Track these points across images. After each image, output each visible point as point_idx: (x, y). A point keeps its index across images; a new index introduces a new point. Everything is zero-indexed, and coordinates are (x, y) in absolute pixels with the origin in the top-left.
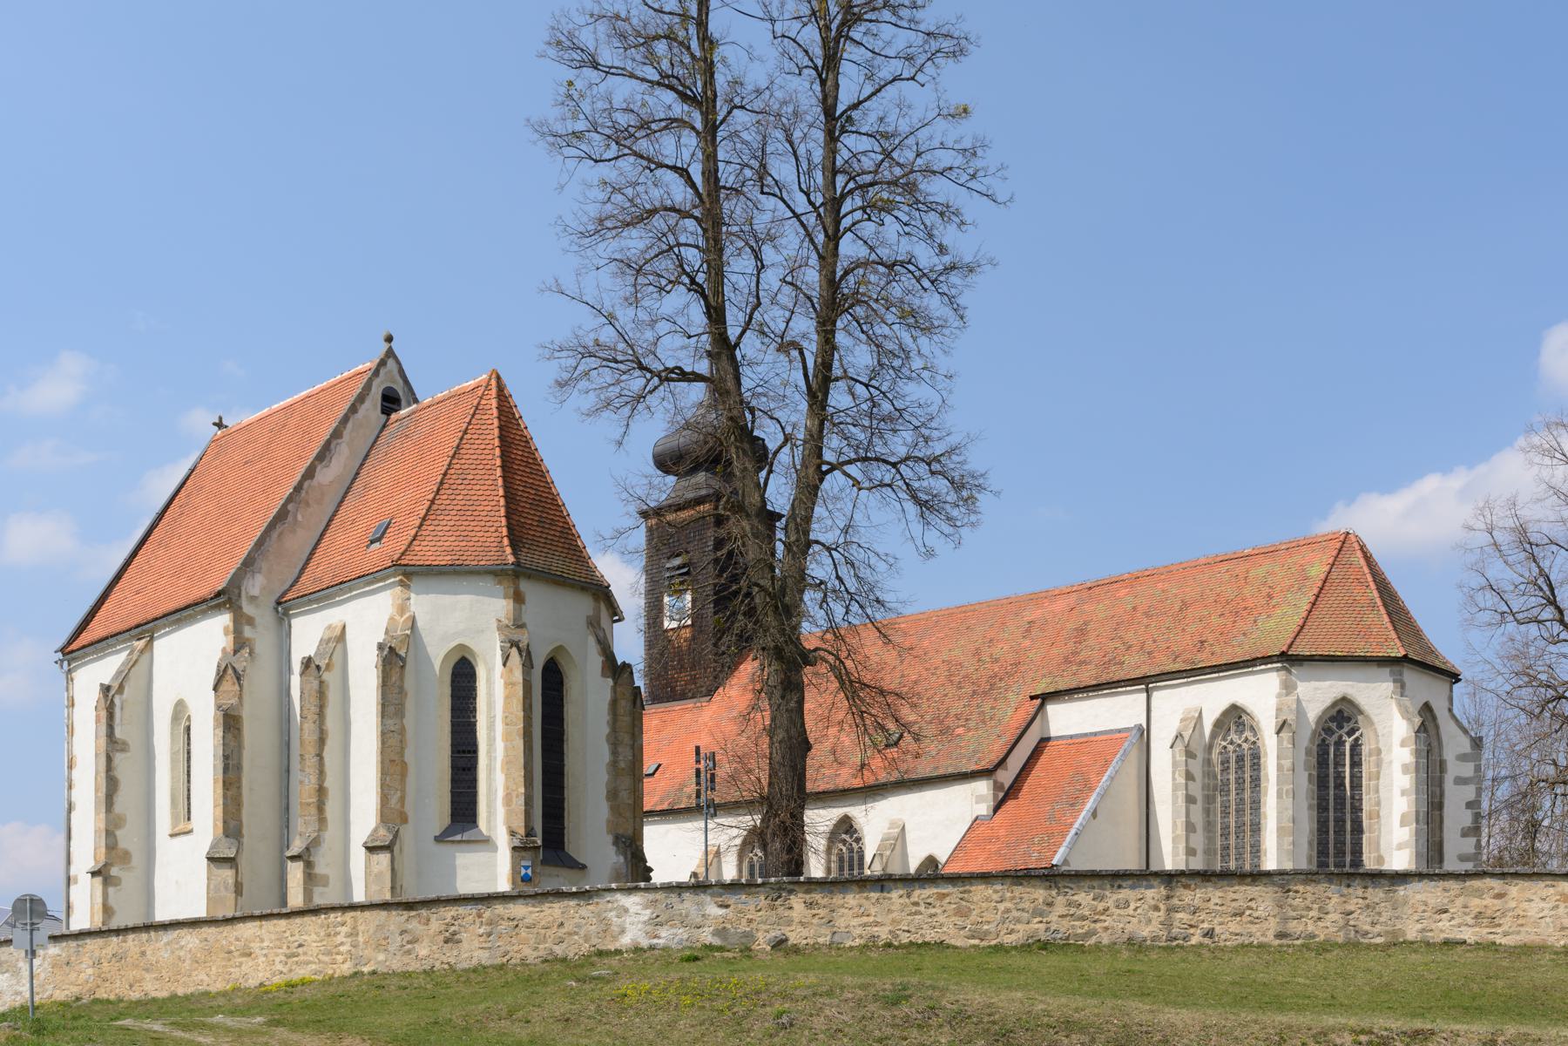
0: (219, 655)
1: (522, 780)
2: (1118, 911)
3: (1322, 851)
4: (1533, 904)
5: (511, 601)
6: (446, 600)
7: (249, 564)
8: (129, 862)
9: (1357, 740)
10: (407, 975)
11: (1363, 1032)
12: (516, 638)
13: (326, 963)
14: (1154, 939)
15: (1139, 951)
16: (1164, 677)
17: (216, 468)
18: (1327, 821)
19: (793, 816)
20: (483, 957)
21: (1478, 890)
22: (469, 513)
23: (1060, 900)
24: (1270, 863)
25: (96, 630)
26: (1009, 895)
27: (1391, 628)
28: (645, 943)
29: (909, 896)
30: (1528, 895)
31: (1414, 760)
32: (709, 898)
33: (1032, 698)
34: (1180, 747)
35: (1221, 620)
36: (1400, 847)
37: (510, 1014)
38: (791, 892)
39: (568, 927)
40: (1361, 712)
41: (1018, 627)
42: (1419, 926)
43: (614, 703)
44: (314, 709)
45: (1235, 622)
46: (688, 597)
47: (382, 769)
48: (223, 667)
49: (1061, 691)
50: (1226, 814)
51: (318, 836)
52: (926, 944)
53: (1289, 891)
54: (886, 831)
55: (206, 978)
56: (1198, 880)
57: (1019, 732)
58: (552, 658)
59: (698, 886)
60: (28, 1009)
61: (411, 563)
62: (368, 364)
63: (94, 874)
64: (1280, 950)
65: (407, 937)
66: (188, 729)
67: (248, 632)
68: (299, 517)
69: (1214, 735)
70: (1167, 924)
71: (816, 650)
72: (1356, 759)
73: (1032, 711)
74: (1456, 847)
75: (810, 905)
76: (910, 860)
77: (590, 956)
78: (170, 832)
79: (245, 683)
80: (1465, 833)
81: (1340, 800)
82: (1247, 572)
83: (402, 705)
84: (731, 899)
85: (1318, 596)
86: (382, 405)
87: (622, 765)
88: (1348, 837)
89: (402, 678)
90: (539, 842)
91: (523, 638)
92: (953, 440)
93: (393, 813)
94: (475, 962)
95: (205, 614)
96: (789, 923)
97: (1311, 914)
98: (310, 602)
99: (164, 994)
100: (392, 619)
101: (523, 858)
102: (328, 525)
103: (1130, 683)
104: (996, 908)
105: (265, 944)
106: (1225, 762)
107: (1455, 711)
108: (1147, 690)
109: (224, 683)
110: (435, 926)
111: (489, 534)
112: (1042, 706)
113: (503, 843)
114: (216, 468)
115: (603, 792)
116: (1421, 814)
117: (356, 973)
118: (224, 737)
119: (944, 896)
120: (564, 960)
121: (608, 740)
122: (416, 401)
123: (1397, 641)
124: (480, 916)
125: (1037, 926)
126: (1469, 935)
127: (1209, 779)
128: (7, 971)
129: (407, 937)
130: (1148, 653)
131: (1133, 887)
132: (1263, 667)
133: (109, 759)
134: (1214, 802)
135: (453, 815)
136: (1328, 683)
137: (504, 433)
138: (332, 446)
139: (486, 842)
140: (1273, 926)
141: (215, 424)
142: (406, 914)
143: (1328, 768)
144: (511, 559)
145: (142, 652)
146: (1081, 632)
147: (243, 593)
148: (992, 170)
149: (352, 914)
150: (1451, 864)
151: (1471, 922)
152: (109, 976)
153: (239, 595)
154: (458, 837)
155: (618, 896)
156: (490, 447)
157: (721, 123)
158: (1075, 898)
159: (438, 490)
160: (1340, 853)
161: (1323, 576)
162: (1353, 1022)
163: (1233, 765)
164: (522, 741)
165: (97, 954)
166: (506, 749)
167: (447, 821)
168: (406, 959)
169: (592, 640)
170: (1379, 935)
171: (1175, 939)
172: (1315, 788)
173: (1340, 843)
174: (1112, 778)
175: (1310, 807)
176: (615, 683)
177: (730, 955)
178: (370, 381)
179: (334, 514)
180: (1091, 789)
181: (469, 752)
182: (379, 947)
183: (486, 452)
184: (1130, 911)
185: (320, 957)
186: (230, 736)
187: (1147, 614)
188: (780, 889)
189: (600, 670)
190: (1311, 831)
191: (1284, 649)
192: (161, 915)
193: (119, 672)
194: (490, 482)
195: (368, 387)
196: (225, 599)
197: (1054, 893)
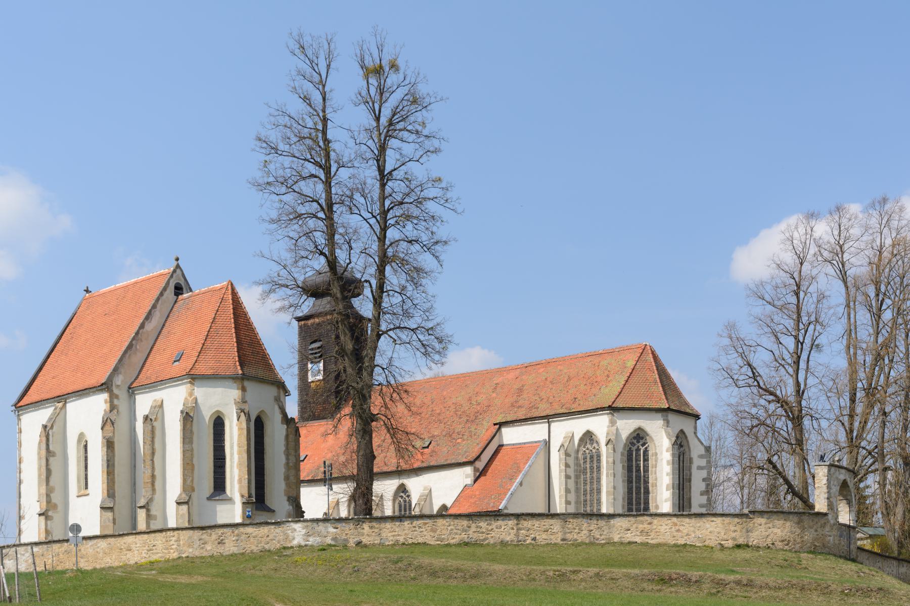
0: (103, 413)
2: (497, 530)
3: (630, 503)
4: (662, 527)
5: (240, 391)
6: (211, 390)
7: (116, 370)
8: (57, 509)
9: (646, 448)
10: (202, 558)
11: (558, 571)
12: (243, 408)
13: (165, 553)
14: (512, 541)
15: (504, 546)
16: (556, 416)
17: (88, 315)
19: (367, 489)
20: (235, 550)
21: (642, 521)
22: (220, 350)
24: (604, 510)
25: (31, 397)
26: (452, 523)
27: (663, 394)
28: (303, 543)
29: (412, 524)
30: (661, 523)
31: (671, 458)
32: (330, 525)
33: (495, 424)
34: (562, 451)
35: (585, 387)
36: (666, 501)
37: (254, 568)
38: (363, 522)
41: (490, 386)
43: (287, 436)
44: (150, 439)
45: (591, 388)
46: (321, 365)
47: (184, 467)
48: (105, 419)
50: (585, 484)
52: (419, 543)
53: (566, 521)
54: (422, 492)
55: (110, 560)
56: (530, 517)
57: (487, 442)
59: (326, 520)
60: (33, 573)
62: (167, 270)
63: (40, 515)
64: (561, 546)
65: (202, 542)
67: (116, 402)
68: (138, 347)
69: (579, 445)
70: (517, 535)
71: (378, 414)
72: (646, 458)
73: (494, 431)
74: (697, 501)
75: (371, 528)
77: (280, 549)
78: (77, 495)
80: (702, 494)
81: (638, 478)
82: (600, 362)
83: (192, 438)
84: (339, 525)
85: (629, 377)
87: (291, 464)
88: (642, 495)
89: (192, 426)
90: (254, 500)
91: (246, 407)
92: (438, 320)
93: (188, 487)
94: (231, 552)
95: (94, 393)
96: (363, 535)
97: (575, 531)
98: (146, 388)
99: (89, 568)
100: (186, 398)
101: (247, 507)
102: (151, 350)
104: (447, 529)
105: (138, 545)
106: (585, 458)
107: (699, 435)
108: (549, 422)
110: (214, 537)
111: (229, 360)
112: (499, 429)
114: (88, 315)
115: (282, 477)
117: (179, 557)
118: (107, 452)
119: (426, 523)
120: (269, 551)
121: (284, 453)
122: (191, 290)
123: (665, 400)
124: (233, 532)
125: (464, 536)
126: (638, 539)
128: (12, 559)
129: (202, 542)
130: (550, 403)
131: (503, 520)
132: (601, 412)
133: (47, 460)
134: (580, 478)
136: (632, 421)
138: (152, 313)
139: (230, 500)
140: (560, 536)
141: (85, 290)
144: (240, 372)
145: (61, 409)
146: (520, 390)
147: (114, 384)
148: (454, 199)
149: (178, 532)
150: (695, 509)
151: (639, 534)
152: (63, 560)
153: (112, 385)
154: (217, 498)
155: (292, 524)
156: (229, 318)
157: (334, 176)
158: (480, 524)
159: (206, 339)
160: (638, 503)
161: (632, 367)
162: (555, 568)
163: (588, 460)
164: (246, 455)
166: (239, 458)
167: (212, 490)
168: (202, 551)
169: (277, 407)
170: (603, 540)
171: (520, 541)
173: (638, 499)
174: (530, 466)
175: (623, 481)
176: (288, 427)
177: (338, 548)
178: (169, 280)
179: (154, 345)
180: (520, 472)
182: (189, 546)
183: (227, 320)
184: (502, 530)
185: (163, 550)
186: (109, 451)
188: (359, 521)
189: (280, 421)
190: (624, 493)
191: (610, 404)
193: (50, 419)
194: (229, 335)
195: (168, 283)
197: (471, 522)
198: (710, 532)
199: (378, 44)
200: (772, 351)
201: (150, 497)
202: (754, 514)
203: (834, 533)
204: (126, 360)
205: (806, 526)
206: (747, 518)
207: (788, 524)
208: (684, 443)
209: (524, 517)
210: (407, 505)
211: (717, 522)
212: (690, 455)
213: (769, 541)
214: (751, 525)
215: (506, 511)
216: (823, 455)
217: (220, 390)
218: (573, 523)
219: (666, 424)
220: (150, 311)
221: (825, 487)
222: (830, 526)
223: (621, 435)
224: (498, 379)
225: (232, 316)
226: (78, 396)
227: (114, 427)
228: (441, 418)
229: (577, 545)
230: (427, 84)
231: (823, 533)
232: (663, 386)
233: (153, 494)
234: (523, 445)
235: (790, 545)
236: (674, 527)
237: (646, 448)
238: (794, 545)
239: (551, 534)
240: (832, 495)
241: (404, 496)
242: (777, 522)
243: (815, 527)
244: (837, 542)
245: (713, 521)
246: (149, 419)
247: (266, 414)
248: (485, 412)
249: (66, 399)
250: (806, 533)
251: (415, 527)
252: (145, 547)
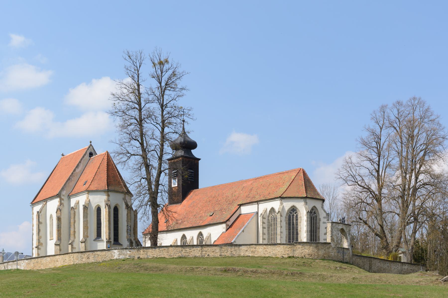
0: (57, 206)
3: (289, 239)
7: (63, 189)
9: (297, 215)
14: (199, 256)
20: (93, 261)
28: (118, 258)
30: (259, 248)
33: (238, 205)
38: (140, 249)
40: (297, 209)
42: (243, 253)
43: (127, 214)
51: (74, 240)
52: (162, 257)
56: (207, 246)
65: (81, 258)
66: (53, 219)
67: (62, 202)
68: (73, 179)
69: (269, 214)
70: (201, 254)
72: (297, 219)
75: (144, 251)
79: (62, 211)
88: (295, 236)
89: (87, 211)
91: (109, 203)
93: (86, 236)
96: (140, 254)
98: (73, 196)
100: (86, 200)
101: (108, 244)
102: (78, 180)
104: (173, 251)
110: (86, 256)
112: (240, 207)
113: (105, 240)
119: (165, 249)
122: (96, 154)
124: (93, 254)
125: (180, 255)
126: (250, 255)
129: (81, 258)
131: (196, 248)
133: (39, 226)
134: (270, 228)
136: (290, 203)
139: (103, 241)
140: (219, 254)
144: (107, 189)
145: (45, 205)
151: (251, 253)
153: (61, 195)
154: (98, 240)
155: (114, 250)
161: (293, 179)
162: (190, 266)
163: (273, 220)
167: (96, 237)
168: (81, 261)
173: (293, 237)
175: (286, 229)
178: (87, 151)
182: (77, 260)
187: (263, 186)
190: (286, 235)
191: (280, 196)
192: (48, 254)
197: (183, 249)
198: (278, 251)
199: (158, 53)
200: (368, 169)
203: (334, 251)
204: (67, 185)
206: (293, 245)
207: (311, 247)
210: (201, 241)
213: (303, 255)
214: (295, 248)
215: (235, 243)
216: (344, 217)
217: (99, 196)
218: (225, 248)
220: (78, 164)
223: (285, 209)
225: (106, 165)
227: (61, 212)
229: (225, 257)
231: (328, 251)
232: (305, 187)
237: (297, 215)
238: (314, 256)
241: (202, 237)
242: (306, 247)
244: (336, 255)
245: (279, 247)
247: (119, 205)
248: (236, 199)
249: (47, 201)
251: (160, 251)
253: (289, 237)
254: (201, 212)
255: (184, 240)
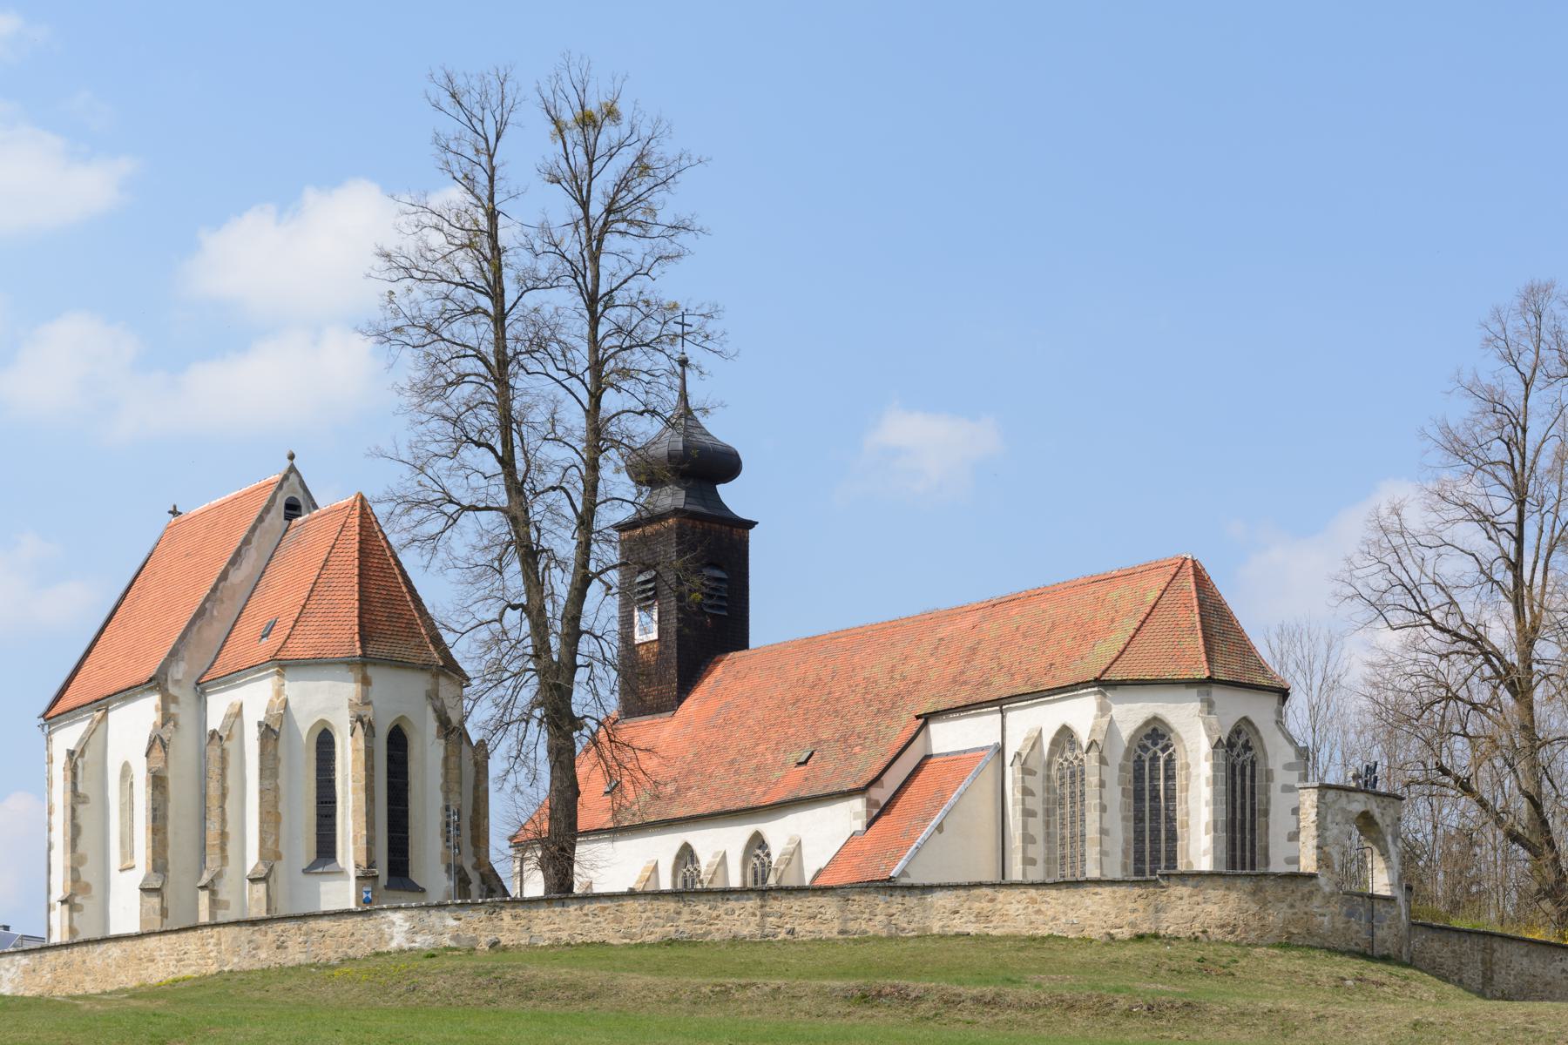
1: (364, 824)
2: (727, 917)
3: (1139, 859)
4: (1012, 906)
5: (360, 684)
6: (311, 685)
7: (174, 654)
9: (1170, 755)
12: (362, 713)
14: (752, 936)
18: (1143, 831)
19: (563, 849)
20: (301, 958)
21: (978, 896)
23: (686, 910)
26: (649, 907)
28: (406, 946)
29: (581, 909)
30: (1009, 899)
33: (918, 717)
36: (1204, 855)
38: (502, 908)
39: (357, 936)
40: (1172, 731)
42: (941, 923)
49: (938, 712)
51: (221, 870)
52: (592, 943)
53: (848, 900)
56: (783, 894)
58: (397, 726)
61: (284, 657)
66: (132, 784)
67: (173, 708)
68: (215, 613)
69: (1052, 753)
70: (762, 926)
72: (1170, 773)
75: (515, 917)
76: (806, 873)
79: (170, 750)
81: (1155, 812)
84: (463, 914)
86: (285, 513)
88: (1163, 845)
89: (276, 748)
91: (368, 713)
93: (271, 854)
94: (297, 961)
97: (865, 916)
98: (219, 684)
100: (271, 701)
101: (365, 885)
102: (238, 617)
103: (990, 704)
104: (640, 917)
105: (164, 952)
108: (1001, 711)
109: (154, 751)
110: (271, 936)
112: (925, 724)
113: (352, 872)
116: (1220, 823)
119: (605, 908)
122: (315, 507)
124: (300, 929)
125: (670, 930)
126: (972, 929)
127: (1048, 793)
131: (737, 900)
132: (1085, 691)
133: (73, 810)
134: (1055, 815)
135: (319, 852)
136: (1139, 705)
137: (363, 546)
138: (243, 551)
139: (341, 873)
140: (836, 925)
141: (170, 512)
142: (252, 929)
143: (1144, 782)
144: (359, 652)
145: (99, 722)
147: (169, 679)
149: (218, 929)
151: (973, 920)
153: (166, 680)
154: (320, 870)
155: (389, 913)
158: (697, 908)
159: (309, 596)
161: (1152, 604)
163: (1068, 780)
165: (53, 963)
167: (313, 856)
168: (252, 961)
170: (913, 930)
171: (767, 936)
172: (1132, 801)
174: (961, 796)
175: (1124, 819)
181: (330, 803)
182: (234, 953)
183: (348, 563)
184: (735, 917)
186: (157, 793)
188: (495, 906)
189: (435, 733)
190: (1126, 841)
191: (1097, 675)
192: (113, 932)
194: (349, 588)
196: (156, 683)
197: (681, 905)
200: (1473, 555)
201: (218, 869)
202: (1168, 879)
205: (1270, 898)
207: (1233, 895)
208: (1253, 742)
209: (773, 893)
210: (762, 872)
211: (1103, 896)
212: (1266, 765)
213: (1197, 927)
215: (904, 881)
216: (1372, 765)
218: (860, 901)
219: (1206, 709)
221: (1313, 827)
222: (1324, 897)
223: (1119, 733)
224: (944, 631)
226: (123, 699)
227: (166, 753)
228: (839, 707)
229: (864, 940)
230: (670, 138)
231: (1306, 909)
232: (1205, 638)
233: (222, 865)
234: (962, 756)
235: (1237, 933)
236: (1031, 906)
237: (1170, 755)
238: (1246, 932)
239: (822, 923)
240: (1330, 840)
241: (762, 855)
242: (1211, 893)
243: (1289, 899)
244: (1340, 925)
245: (1096, 894)
246: (217, 737)
248: (910, 693)
249: (108, 705)
250: (1271, 911)
251: (586, 915)
252: (172, 955)
253: (1135, 852)
254: (761, 748)
255: (689, 866)
